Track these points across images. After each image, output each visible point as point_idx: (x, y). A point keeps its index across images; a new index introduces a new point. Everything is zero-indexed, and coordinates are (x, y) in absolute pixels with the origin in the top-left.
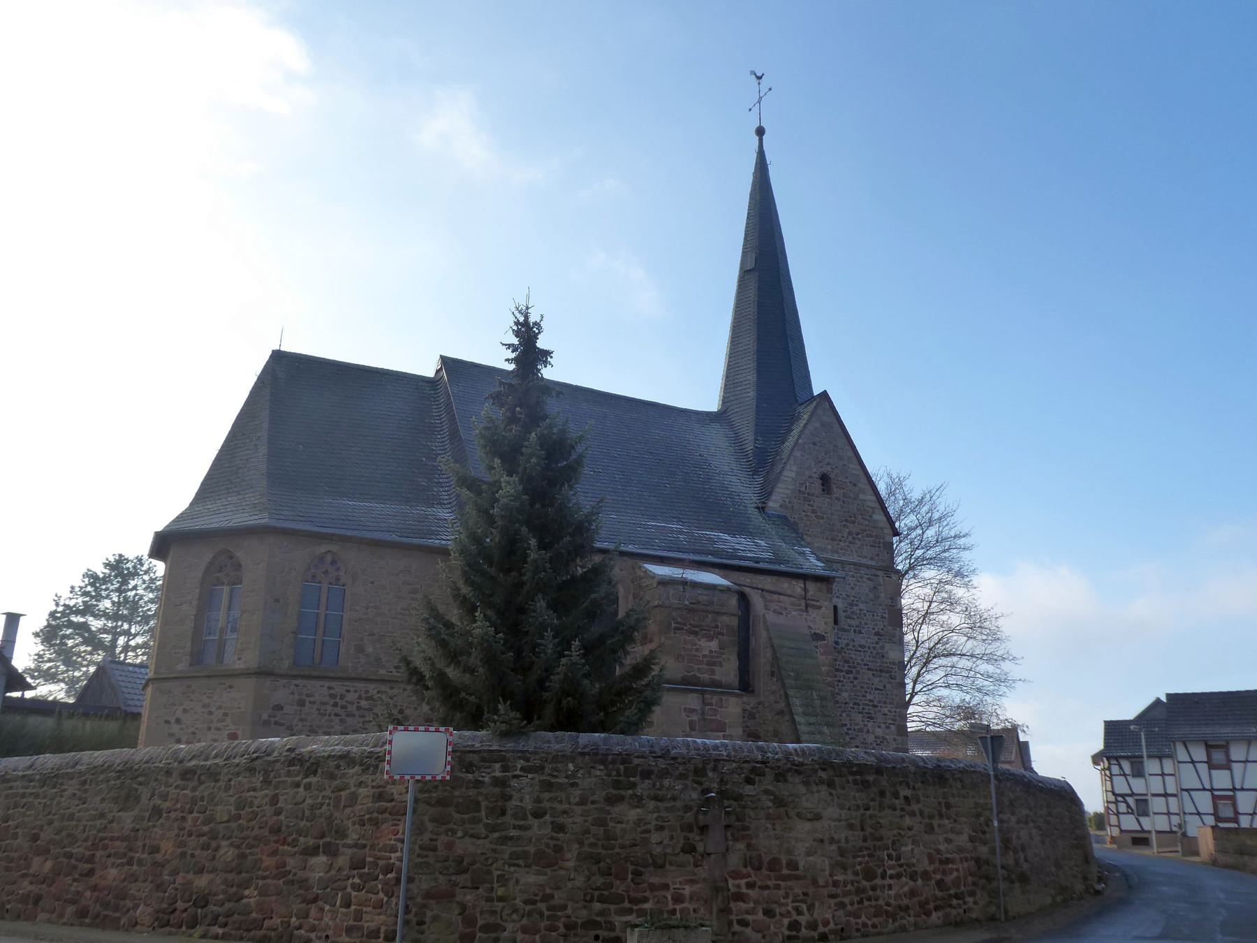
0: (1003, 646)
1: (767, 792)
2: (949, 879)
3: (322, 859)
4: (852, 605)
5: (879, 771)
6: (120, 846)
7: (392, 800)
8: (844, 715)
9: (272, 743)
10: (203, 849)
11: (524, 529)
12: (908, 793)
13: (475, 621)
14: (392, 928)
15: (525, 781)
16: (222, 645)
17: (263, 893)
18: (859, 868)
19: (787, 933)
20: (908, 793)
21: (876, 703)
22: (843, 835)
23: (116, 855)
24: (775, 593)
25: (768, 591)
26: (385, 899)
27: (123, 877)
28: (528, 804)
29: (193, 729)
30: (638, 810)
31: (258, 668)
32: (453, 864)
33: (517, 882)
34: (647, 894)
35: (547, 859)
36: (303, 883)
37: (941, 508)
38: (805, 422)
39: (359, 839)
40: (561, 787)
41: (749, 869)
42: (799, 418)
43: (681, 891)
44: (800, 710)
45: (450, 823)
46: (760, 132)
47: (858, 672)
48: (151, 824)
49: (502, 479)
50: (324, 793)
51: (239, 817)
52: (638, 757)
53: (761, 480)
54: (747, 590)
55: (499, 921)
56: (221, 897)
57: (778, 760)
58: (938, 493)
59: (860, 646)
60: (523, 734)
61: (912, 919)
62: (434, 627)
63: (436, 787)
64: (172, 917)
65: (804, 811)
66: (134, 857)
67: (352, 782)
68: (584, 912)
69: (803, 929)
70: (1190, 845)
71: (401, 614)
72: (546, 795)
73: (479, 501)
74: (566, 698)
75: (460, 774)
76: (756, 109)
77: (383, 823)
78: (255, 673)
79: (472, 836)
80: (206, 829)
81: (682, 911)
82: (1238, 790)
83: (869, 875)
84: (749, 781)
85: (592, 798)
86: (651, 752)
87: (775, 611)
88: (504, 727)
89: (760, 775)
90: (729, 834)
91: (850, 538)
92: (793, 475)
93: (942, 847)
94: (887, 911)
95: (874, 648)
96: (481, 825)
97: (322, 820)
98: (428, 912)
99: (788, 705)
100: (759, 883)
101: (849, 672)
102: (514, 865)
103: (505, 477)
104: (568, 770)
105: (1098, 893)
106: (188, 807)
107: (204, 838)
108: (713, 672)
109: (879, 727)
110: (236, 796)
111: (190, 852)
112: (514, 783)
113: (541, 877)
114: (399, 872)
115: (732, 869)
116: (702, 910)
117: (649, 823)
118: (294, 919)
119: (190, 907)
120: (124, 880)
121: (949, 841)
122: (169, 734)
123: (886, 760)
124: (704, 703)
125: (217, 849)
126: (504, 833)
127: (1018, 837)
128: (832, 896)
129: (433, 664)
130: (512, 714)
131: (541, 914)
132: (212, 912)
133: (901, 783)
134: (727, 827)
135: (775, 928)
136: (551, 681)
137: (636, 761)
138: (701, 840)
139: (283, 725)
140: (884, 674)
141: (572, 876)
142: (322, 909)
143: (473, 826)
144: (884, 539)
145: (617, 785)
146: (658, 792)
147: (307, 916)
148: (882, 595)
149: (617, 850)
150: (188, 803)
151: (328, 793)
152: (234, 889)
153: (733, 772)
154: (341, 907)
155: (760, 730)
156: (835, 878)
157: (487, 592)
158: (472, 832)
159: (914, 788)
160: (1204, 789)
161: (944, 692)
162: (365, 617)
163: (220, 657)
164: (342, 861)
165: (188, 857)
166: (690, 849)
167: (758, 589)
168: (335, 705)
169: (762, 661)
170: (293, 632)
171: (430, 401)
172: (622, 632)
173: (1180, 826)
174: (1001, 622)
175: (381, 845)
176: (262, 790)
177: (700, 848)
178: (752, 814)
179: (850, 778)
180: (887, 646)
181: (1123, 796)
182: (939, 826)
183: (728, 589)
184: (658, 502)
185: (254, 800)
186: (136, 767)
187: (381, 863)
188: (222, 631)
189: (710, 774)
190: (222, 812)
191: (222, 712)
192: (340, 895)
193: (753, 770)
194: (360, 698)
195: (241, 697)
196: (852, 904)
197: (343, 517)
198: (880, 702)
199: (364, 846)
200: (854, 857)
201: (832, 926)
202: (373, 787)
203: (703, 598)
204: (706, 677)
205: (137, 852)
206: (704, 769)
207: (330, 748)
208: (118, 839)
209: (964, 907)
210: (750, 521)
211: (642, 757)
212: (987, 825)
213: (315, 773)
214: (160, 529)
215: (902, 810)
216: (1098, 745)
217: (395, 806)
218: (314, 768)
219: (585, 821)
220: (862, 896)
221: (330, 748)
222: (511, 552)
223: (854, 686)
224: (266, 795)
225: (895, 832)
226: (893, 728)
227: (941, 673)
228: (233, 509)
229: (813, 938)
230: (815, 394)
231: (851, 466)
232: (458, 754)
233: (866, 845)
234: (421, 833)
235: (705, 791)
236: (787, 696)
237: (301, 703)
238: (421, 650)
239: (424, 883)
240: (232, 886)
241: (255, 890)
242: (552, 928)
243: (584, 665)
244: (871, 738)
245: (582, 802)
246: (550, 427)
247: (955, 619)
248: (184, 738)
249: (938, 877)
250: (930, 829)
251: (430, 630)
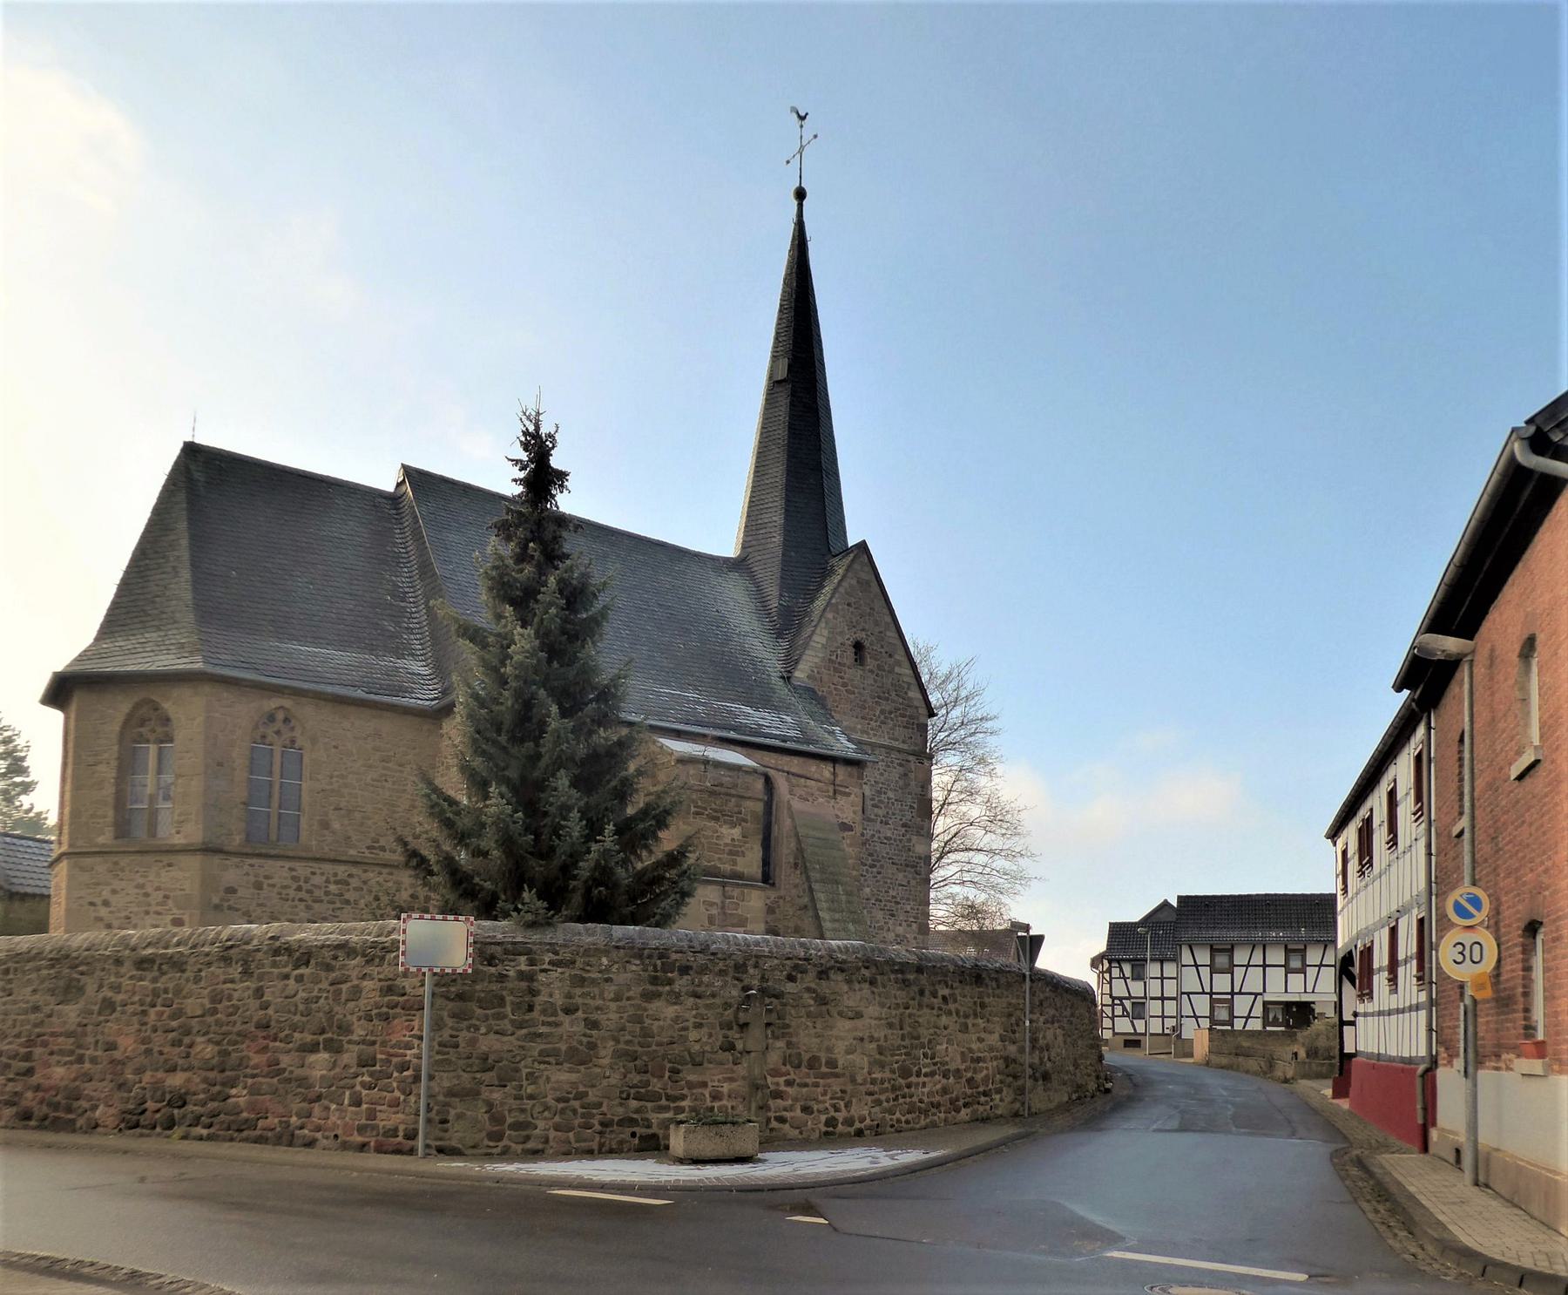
0: (1022, 841)
1: (808, 990)
2: (979, 1077)
3: (323, 1056)
4: (879, 792)
5: (920, 970)
6: (66, 1043)
7: (404, 995)
8: (865, 911)
9: (249, 930)
10: (173, 1045)
11: (542, 693)
12: (946, 992)
13: (490, 798)
14: (413, 1126)
15: (553, 975)
16: (153, 814)
17: (254, 1091)
18: (896, 1066)
19: (824, 1129)
20: (946, 992)
21: (898, 900)
22: (882, 1034)
23: (61, 1052)
24: (801, 776)
25: (793, 774)
26: (402, 1097)
27: (73, 1075)
28: (559, 999)
30: (676, 1007)
31: (204, 843)
32: (477, 1061)
33: (548, 1079)
34: (685, 1091)
35: (581, 1056)
36: (303, 1082)
37: (969, 686)
38: (839, 577)
39: (367, 1035)
40: (594, 982)
41: (788, 1067)
42: (832, 572)
43: (719, 1089)
44: (825, 905)
45: (471, 1018)
46: (800, 194)
47: (882, 866)
48: (102, 1018)
49: (515, 632)
50: (320, 986)
51: (214, 1012)
52: (676, 952)
53: (785, 644)
54: (772, 772)
55: (530, 1119)
56: (202, 1096)
57: (821, 957)
58: (966, 669)
59: (885, 838)
60: (549, 924)
61: (942, 1115)
62: (437, 804)
63: (454, 980)
64: (142, 1118)
65: (845, 1009)
66: (84, 1054)
67: (354, 974)
68: (621, 1110)
69: (840, 1125)
70: (1185, 1048)
71: (373, 786)
72: (578, 991)
73: (487, 657)
74: (596, 888)
75: (481, 967)
76: (796, 162)
77: (394, 1018)
78: (199, 850)
79: (497, 1033)
80: (174, 1024)
81: (720, 1108)
82: (1237, 994)
83: (905, 1072)
84: (791, 978)
85: (627, 995)
86: (690, 947)
87: (800, 797)
88: (529, 917)
89: (801, 973)
90: (769, 1032)
91: (882, 717)
92: (824, 641)
93: (974, 1046)
94: (920, 1108)
95: (900, 840)
96: (506, 1021)
97: (321, 1014)
98: (451, 1110)
99: (813, 899)
100: (798, 1081)
101: (872, 866)
102: (545, 1063)
103: (519, 629)
104: (601, 965)
105: (1108, 1091)
106: (148, 1000)
107: (174, 1033)
108: (735, 863)
109: (900, 925)
110: (210, 989)
111: (156, 1049)
112: (542, 977)
113: (574, 1075)
114: (418, 1070)
115: (772, 1067)
116: (741, 1107)
117: (687, 1021)
118: (294, 1119)
119: (164, 1106)
120: (75, 1080)
121: (980, 1040)
123: (928, 959)
124: (725, 896)
125: (191, 1046)
126: (532, 1030)
127: (1044, 1037)
128: (871, 1094)
129: (438, 846)
130: (539, 904)
131: (575, 1111)
132: (192, 1112)
133: (940, 982)
134: (768, 1025)
135: (812, 1124)
136: (580, 868)
137: (674, 956)
138: (741, 1038)
139: (237, 910)
140: (909, 869)
141: (607, 1074)
142: (328, 1108)
143: (497, 1022)
144: (918, 719)
145: (654, 981)
146: (697, 989)
147: (309, 1116)
148: (913, 783)
149: (654, 1047)
150: (148, 996)
151: (325, 985)
152: (218, 1088)
153: (773, 969)
154: (350, 1105)
155: (780, 926)
156: (874, 1076)
157: (502, 764)
158: (495, 1028)
159: (952, 987)
160: (1188, 994)
161: (956, 889)
162: (328, 787)
163: (152, 830)
164: (349, 1057)
165: (156, 1055)
166: (729, 1047)
167: (784, 771)
168: (299, 889)
169: (785, 851)
170: (244, 803)
171: (391, 523)
172: (654, 817)
173: (1174, 1029)
174: (1023, 815)
175: (394, 1042)
176: (242, 982)
177: (739, 1046)
178: (793, 1012)
179: (892, 976)
180: (914, 838)
181: (1121, 999)
182: (973, 1025)
183: (755, 771)
184: (671, 665)
185: (232, 992)
186: (74, 954)
187: (395, 1060)
188: (152, 799)
189: (751, 971)
190: (193, 1006)
192: (347, 1093)
193: (796, 967)
194: (328, 881)
195: (186, 876)
196: (888, 1101)
197: (296, 666)
198: (902, 898)
199: (374, 1043)
200: (892, 1055)
201: (868, 1121)
202: (380, 980)
203: (726, 780)
204: (727, 868)
205: (88, 1049)
206: (744, 965)
207: (323, 937)
208: (61, 1035)
209: (992, 1104)
210: (775, 693)
211: (681, 952)
212: (1018, 1025)
213: (307, 964)
214: (60, 669)
215: (940, 1009)
216: (1101, 946)
217: (408, 1000)
218: (306, 957)
219: (621, 1018)
220: (898, 1093)
221: (323, 937)
222: (526, 724)
223: (877, 881)
224: (248, 988)
225: (932, 1031)
226: (914, 925)
227: (954, 869)
228: (155, 648)
229: (850, 1133)
230: (850, 545)
231: (888, 634)
232: (478, 946)
233: (903, 1043)
234: (440, 1029)
235: (746, 989)
236: (811, 890)
237: (258, 886)
238: (426, 833)
239: (446, 1081)
240: (215, 1085)
241: (245, 1088)
242: (588, 1126)
243: (619, 852)
244: (891, 936)
245: (617, 998)
246: (570, 569)
247: (975, 811)
248: (116, 923)
249: (969, 1075)
250: (964, 1029)
251: (432, 807)
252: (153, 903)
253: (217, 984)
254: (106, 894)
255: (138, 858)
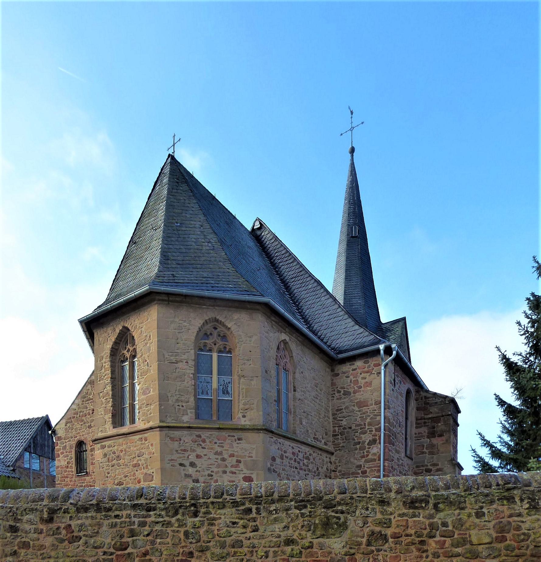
29: (209, 472)
31: (263, 425)
46: (352, 150)
91: (70, 431)
122: (186, 475)
185: (520, 524)
191: (235, 459)
252: (229, 465)
253: (503, 518)
254: (192, 458)
255: (216, 433)
